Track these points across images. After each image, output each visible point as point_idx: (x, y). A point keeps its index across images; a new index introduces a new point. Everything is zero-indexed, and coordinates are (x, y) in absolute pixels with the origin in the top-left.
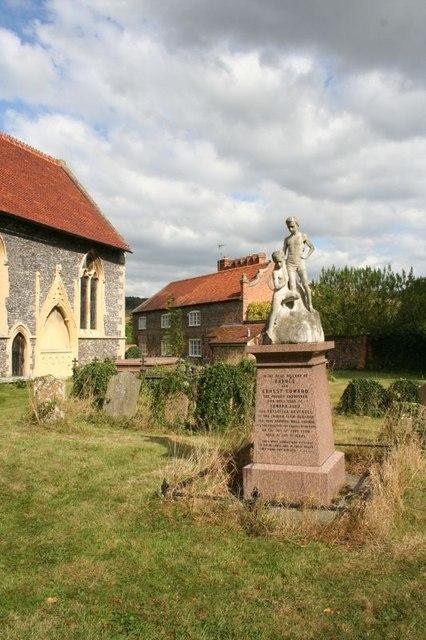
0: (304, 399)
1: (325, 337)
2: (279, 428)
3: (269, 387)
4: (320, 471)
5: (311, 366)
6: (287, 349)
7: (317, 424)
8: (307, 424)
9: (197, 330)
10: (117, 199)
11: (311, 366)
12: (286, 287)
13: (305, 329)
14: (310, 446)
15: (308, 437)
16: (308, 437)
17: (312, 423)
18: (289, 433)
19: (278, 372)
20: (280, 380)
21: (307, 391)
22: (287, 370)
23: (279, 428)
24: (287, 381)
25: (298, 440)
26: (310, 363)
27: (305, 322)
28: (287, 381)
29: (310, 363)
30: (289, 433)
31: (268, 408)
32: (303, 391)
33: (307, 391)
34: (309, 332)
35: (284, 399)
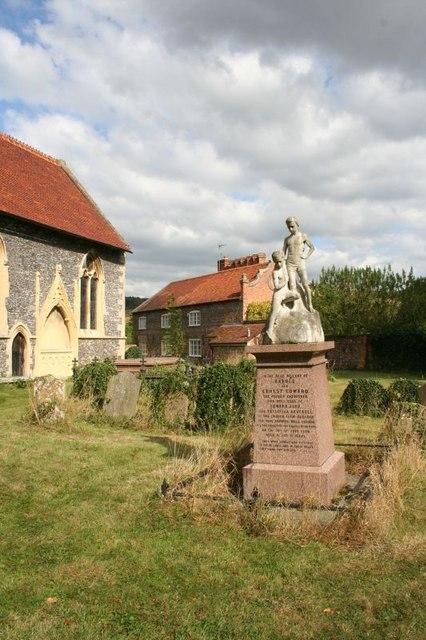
0: (304, 399)
1: (325, 337)
2: (279, 428)
3: (269, 387)
4: (320, 471)
5: (311, 366)
6: (287, 349)
7: (317, 424)
8: (307, 424)
9: (197, 330)
10: (117, 199)
11: (311, 366)
12: (286, 287)
13: (305, 329)
14: (310, 446)
15: (308, 437)
16: (308, 437)
17: (312, 423)
18: (289, 433)
19: (278, 372)
20: (280, 380)
21: (307, 391)
22: (287, 370)
23: (279, 428)
24: (287, 381)
25: (298, 440)
26: (310, 363)
27: (305, 322)
28: (287, 381)
29: (310, 363)
30: (289, 433)
31: (268, 408)
32: (303, 391)
33: (307, 391)
34: (309, 332)
35: (284, 399)
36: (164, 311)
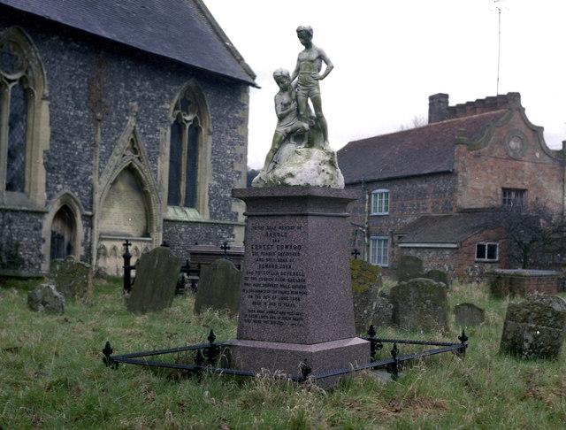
14: (298, 318)
19: (270, 222)
21: (300, 247)
22: (280, 220)
33: (300, 247)
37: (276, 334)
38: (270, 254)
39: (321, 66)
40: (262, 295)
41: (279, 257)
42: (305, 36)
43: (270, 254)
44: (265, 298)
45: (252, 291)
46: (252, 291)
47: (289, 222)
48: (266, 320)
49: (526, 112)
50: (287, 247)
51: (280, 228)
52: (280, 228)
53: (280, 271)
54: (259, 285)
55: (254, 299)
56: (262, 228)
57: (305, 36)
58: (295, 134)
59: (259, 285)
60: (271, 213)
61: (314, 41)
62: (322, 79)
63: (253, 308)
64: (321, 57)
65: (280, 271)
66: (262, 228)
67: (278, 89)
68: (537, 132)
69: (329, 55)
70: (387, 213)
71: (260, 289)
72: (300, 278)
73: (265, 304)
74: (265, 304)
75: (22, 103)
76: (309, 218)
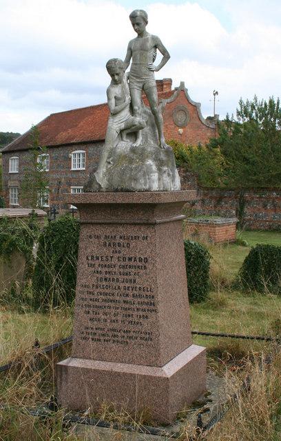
0: (142, 271)
1: (161, 81)
2: (107, 310)
3: (96, 253)
4: (158, 374)
5: (278, 103)
6: (119, 199)
7: (160, 307)
8: (145, 306)
9: (81, 175)
10: (157, 174)
11: (278, 103)
12: (127, 109)
13: (147, 173)
14: (148, 337)
15: (146, 325)
16: (146, 325)
17: (151, 306)
18: (120, 318)
19: (108, 231)
20: (110, 243)
21: (146, 260)
22: (121, 229)
23: (107, 310)
24: (119, 245)
25: (131, 327)
26: (276, 102)
27: (150, 162)
28: (119, 245)
29: (276, 102)
30: (120, 318)
31: (93, 281)
32: (140, 260)
33: (146, 260)
34: (155, 176)
35: (116, 269)
36: (186, 202)
37: (120, 354)
38: (109, 266)
39: (155, 57)
40: (101, 311)
41: (122, 270)
42: (138, 21)
43: (109, 266)
44: (106, 314)
45: (89, 306)
46: (89, 306)
47: (132, 231)
48: (107, 338)
49: (189, 92)
50: (130, 259)
51: (121, 238)
52: (121, 238)
53: (122, 285)
54: (97, 300)
55: (91, 315)
56: (98, 237)
57: (138, 21)
58: (129, 131)
59: (97, 300)
60: (111, 221)
61: (150, 29)
62: (157, 70)
63: (90, 324)
64: (157, 45)
65: (122, 285)
66: (98, 237)
67: (109, 79)
68: (196, 107)
69: (166, 43)
70: (84, 169)
71: (97, 304)
72: (148, 293)
73: (105, 320)
74: (105, 320)
75: (217, 228)
76: (157, 228)
